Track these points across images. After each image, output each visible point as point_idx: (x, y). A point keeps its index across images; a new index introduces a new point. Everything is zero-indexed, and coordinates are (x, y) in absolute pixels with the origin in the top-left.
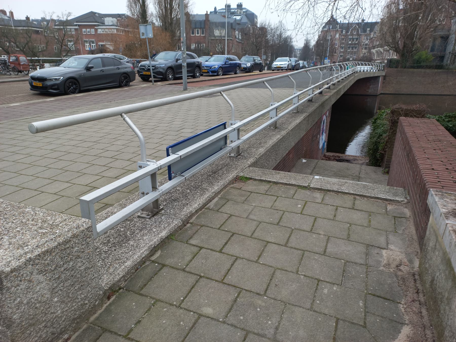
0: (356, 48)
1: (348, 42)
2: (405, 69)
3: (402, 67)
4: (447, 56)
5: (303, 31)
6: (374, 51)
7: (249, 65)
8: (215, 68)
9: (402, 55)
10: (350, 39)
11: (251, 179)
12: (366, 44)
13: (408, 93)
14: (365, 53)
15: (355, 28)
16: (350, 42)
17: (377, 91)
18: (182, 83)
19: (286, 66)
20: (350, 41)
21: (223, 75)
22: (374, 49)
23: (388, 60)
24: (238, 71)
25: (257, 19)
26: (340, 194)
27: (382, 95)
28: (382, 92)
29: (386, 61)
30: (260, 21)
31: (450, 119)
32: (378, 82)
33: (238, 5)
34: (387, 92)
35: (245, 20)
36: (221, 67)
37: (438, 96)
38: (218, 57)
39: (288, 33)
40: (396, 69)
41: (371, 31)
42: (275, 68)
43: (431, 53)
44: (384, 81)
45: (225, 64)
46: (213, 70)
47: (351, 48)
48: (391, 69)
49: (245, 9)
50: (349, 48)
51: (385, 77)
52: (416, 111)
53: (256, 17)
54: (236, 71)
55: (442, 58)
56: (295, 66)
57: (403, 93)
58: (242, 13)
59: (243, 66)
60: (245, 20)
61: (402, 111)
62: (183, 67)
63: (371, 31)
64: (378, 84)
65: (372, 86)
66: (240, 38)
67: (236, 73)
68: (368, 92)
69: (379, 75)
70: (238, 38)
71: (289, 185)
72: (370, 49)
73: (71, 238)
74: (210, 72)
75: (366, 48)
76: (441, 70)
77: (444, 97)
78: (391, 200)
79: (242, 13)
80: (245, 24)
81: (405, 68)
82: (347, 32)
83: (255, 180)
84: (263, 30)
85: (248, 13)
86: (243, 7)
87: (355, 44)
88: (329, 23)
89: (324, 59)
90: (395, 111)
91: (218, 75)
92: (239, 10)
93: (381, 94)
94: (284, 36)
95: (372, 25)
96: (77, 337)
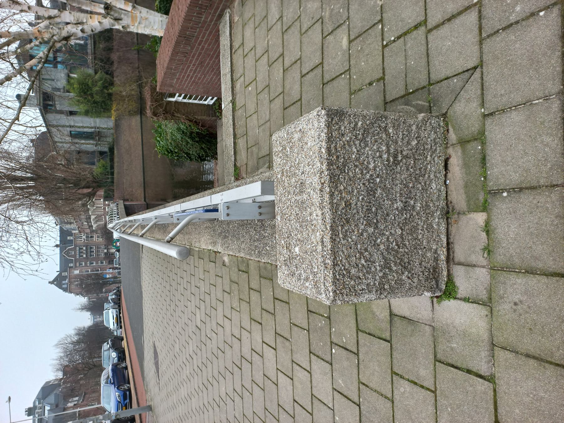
0: (91, 248)
1: (84, 258)
3: (113, 185)
4: (99, 150)
5: (71, 314)
6: (94, 226)
7: (114, 355)
8: (119, 396)
10: (80, 256)
11: (235, 165)
12: (87, 237)
14: (98, 237)
15: (68, 253)
16: (85, 256)
18: (140, 415)
19: (114, 311)
20: (82, 256)
21: (129, 383)
22: (92, 226)
23: (104, 201)
24: (124, 365)
25: (50, 382)
26: (233, 69)
28: (143, 200)
29: (107, 202)
30: (51, 374)
33: (29, 415)
34: (143, 195)
35: (52, 398)
36: (117, 388)
38: (104, 398)
39: (73, 332)
40: (115, 191)
41: (71, 234)
42: (117, 325)
43: (97, 163)
45: (113, 383)
46: (122, 398)
47: (92, 254)
49: (34, 402)
50: (91, 255)
51: (124, 200)
52: (152, 93)
53: (47, 383)
54: (123, 368)
55: (102, 153)
56: (114, 302)
57: (142, 180)
58: (41, 405)
59: (116, 361)
60: (52, 398)
61: (153, 105)
62: (118, 417)
63: (71, 234)
66: (77, 398)
67: (126, 368)
69: (123, 207)
70: (78, 401)
71: (234, 124)
72: (92, 231)
74: (126, 402)
75: (92, 237)
77: (144, 141)
78: (230, 22)
79: (41, 405)
80: (57, 396)
82: (71, 261)
83: (235, 160)
84: (65, 370)
85: (41, 397)
86: (32, 406)
87: (87, 250)
88: (60, 286)
89: (106, 278)
90: (154, 112)
91: (129, 390)
92: (37, 411)
93: (145, 201)
94: (75, 338)
95: (64, 234)
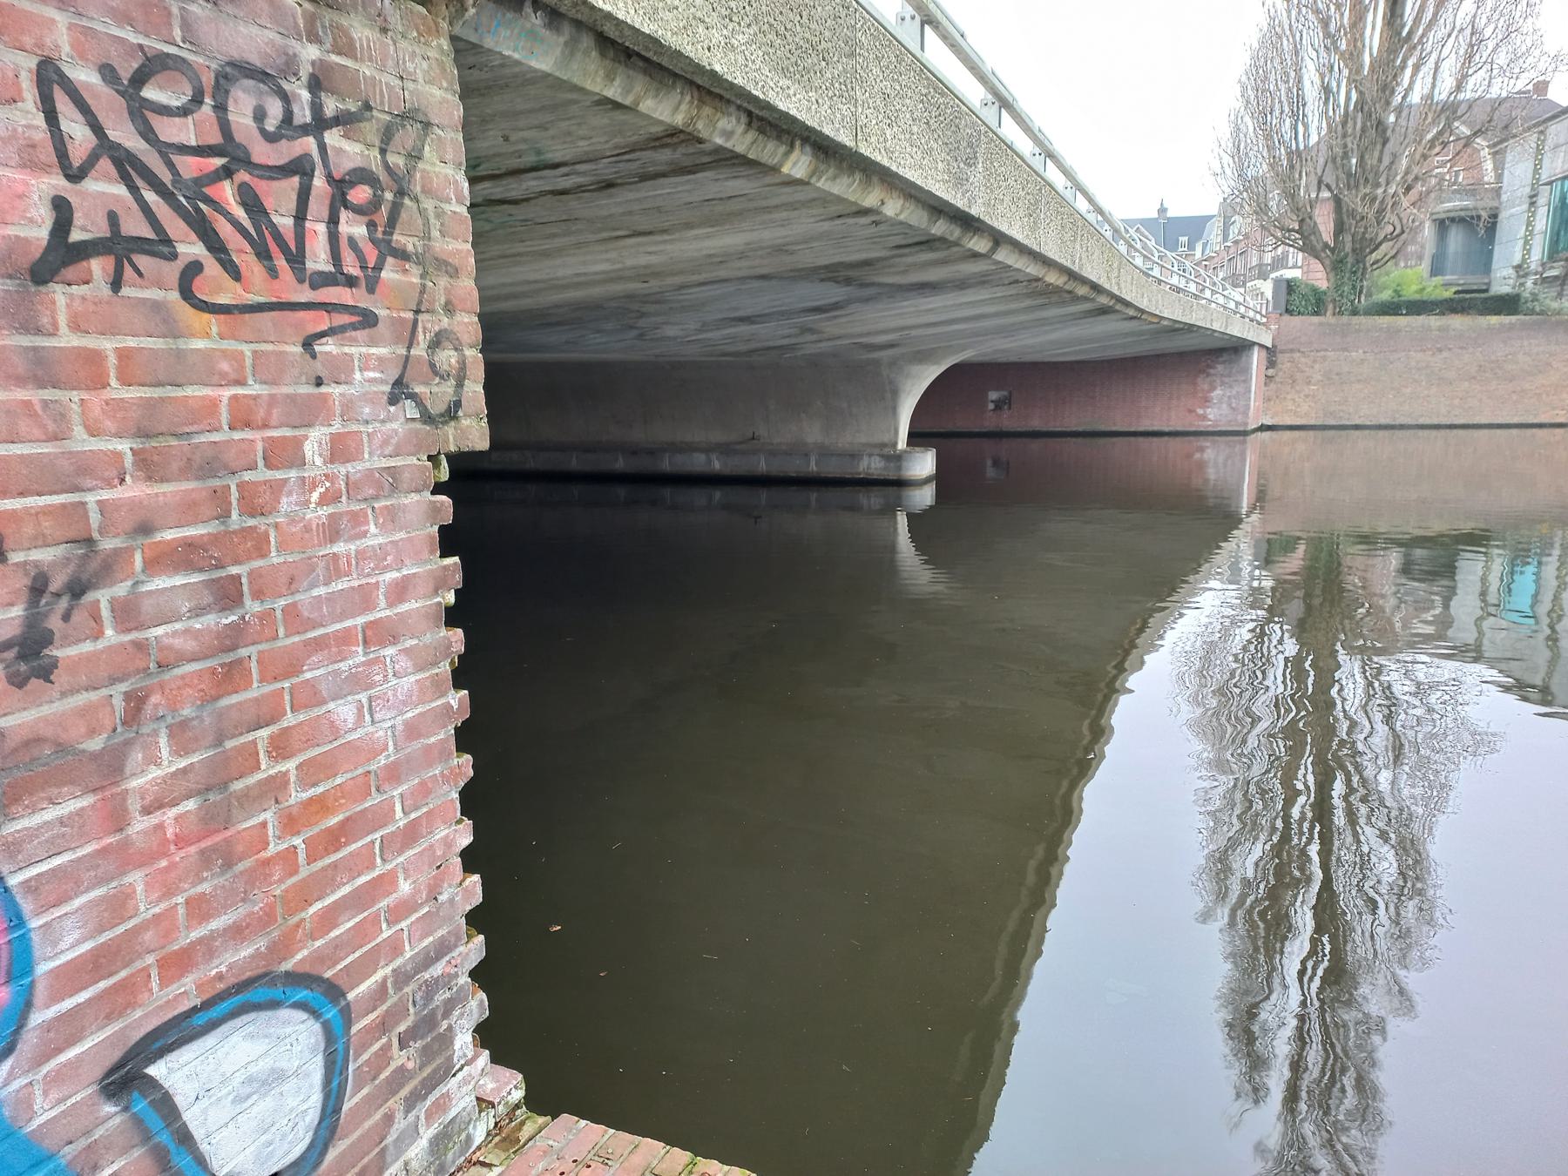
2: (1355, 319)
9: (1337, 266)
13: (1383, 421)
17: (1246, 413)
27: (1266, 435)
31: (1348, 1081)
32: (1246, 370)
37: (1514, 432)
40: (1315, 319)
44: (1271, 372)
48: (1296, 321)
51: (1271, 353)
64: (1247, 381)
65: (1218, 392)
68: (1204, 417)
73: (128, 743)
76: (1513, 318)
81: (1355, 313)
93: (1264, 428)
96: (60, 1018)
